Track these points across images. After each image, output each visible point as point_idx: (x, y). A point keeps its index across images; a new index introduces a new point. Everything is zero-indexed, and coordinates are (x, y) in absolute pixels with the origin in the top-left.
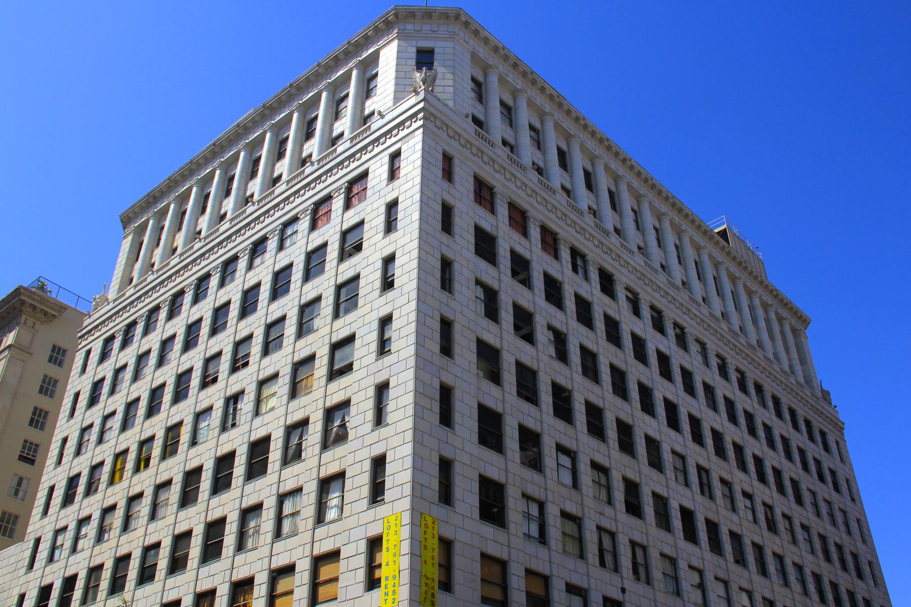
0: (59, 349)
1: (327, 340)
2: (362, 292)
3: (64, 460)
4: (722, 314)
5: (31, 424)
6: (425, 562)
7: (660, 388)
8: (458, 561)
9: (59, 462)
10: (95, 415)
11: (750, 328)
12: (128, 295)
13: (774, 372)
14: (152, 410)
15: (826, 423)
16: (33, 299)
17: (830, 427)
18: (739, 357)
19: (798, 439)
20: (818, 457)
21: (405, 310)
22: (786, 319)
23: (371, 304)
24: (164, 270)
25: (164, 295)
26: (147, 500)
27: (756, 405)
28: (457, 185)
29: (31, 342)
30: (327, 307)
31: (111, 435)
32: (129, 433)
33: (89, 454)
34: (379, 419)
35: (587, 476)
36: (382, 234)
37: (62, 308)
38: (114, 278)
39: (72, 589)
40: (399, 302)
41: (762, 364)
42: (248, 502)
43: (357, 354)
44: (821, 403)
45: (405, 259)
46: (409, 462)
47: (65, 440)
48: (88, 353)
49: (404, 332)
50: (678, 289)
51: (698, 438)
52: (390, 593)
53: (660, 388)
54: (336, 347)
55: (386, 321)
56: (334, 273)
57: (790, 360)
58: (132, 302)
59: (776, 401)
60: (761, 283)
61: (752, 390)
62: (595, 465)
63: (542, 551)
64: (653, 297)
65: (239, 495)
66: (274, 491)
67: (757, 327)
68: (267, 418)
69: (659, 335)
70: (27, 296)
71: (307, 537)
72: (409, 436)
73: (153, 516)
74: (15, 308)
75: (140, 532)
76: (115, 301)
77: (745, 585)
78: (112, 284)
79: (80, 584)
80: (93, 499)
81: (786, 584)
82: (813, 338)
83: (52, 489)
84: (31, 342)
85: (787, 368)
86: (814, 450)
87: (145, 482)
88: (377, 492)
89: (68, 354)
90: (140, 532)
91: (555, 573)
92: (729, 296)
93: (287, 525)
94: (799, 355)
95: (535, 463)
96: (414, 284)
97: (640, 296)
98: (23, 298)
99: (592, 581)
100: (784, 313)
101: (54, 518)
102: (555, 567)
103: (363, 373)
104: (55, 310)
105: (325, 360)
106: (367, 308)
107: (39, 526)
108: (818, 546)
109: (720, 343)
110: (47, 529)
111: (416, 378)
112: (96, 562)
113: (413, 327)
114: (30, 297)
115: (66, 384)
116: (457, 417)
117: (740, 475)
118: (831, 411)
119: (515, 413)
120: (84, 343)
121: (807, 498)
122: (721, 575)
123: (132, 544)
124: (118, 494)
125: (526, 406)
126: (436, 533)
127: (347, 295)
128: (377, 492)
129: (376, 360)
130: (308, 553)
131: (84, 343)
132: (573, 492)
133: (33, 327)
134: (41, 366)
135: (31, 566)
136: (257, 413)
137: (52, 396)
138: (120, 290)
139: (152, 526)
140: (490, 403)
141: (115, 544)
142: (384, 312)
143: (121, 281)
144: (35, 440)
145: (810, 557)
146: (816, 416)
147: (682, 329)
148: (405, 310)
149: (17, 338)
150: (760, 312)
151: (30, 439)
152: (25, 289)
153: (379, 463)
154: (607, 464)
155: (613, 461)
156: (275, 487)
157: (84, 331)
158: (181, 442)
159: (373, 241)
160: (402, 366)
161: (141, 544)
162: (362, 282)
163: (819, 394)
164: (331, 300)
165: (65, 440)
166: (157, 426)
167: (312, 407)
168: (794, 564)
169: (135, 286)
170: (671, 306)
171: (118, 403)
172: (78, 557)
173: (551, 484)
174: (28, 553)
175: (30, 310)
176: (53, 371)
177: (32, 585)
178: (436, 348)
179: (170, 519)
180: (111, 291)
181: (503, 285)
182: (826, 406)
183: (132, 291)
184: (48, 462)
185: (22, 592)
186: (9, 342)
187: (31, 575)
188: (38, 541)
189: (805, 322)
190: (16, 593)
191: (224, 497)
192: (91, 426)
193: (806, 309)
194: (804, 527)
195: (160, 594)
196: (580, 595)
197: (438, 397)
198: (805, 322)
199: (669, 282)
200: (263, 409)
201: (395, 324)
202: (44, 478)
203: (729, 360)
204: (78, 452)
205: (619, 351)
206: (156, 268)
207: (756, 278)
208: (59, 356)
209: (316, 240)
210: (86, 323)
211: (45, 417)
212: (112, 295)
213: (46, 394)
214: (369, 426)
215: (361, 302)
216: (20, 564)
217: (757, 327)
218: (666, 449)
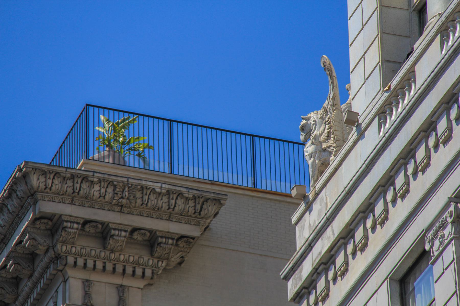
12: (423, 72)
37: (204, 202)
38: (354, 25)
70: (61, 197)
74: (32, 257)
76: (382, 114)
78: (354, 54)
98: (48, 207)
104: (182, 217)
114: (74, 198)
143: (385, 32)
157: (307, 268)
180: (356, 79)
210: (303, 234)
212: (364, 95)
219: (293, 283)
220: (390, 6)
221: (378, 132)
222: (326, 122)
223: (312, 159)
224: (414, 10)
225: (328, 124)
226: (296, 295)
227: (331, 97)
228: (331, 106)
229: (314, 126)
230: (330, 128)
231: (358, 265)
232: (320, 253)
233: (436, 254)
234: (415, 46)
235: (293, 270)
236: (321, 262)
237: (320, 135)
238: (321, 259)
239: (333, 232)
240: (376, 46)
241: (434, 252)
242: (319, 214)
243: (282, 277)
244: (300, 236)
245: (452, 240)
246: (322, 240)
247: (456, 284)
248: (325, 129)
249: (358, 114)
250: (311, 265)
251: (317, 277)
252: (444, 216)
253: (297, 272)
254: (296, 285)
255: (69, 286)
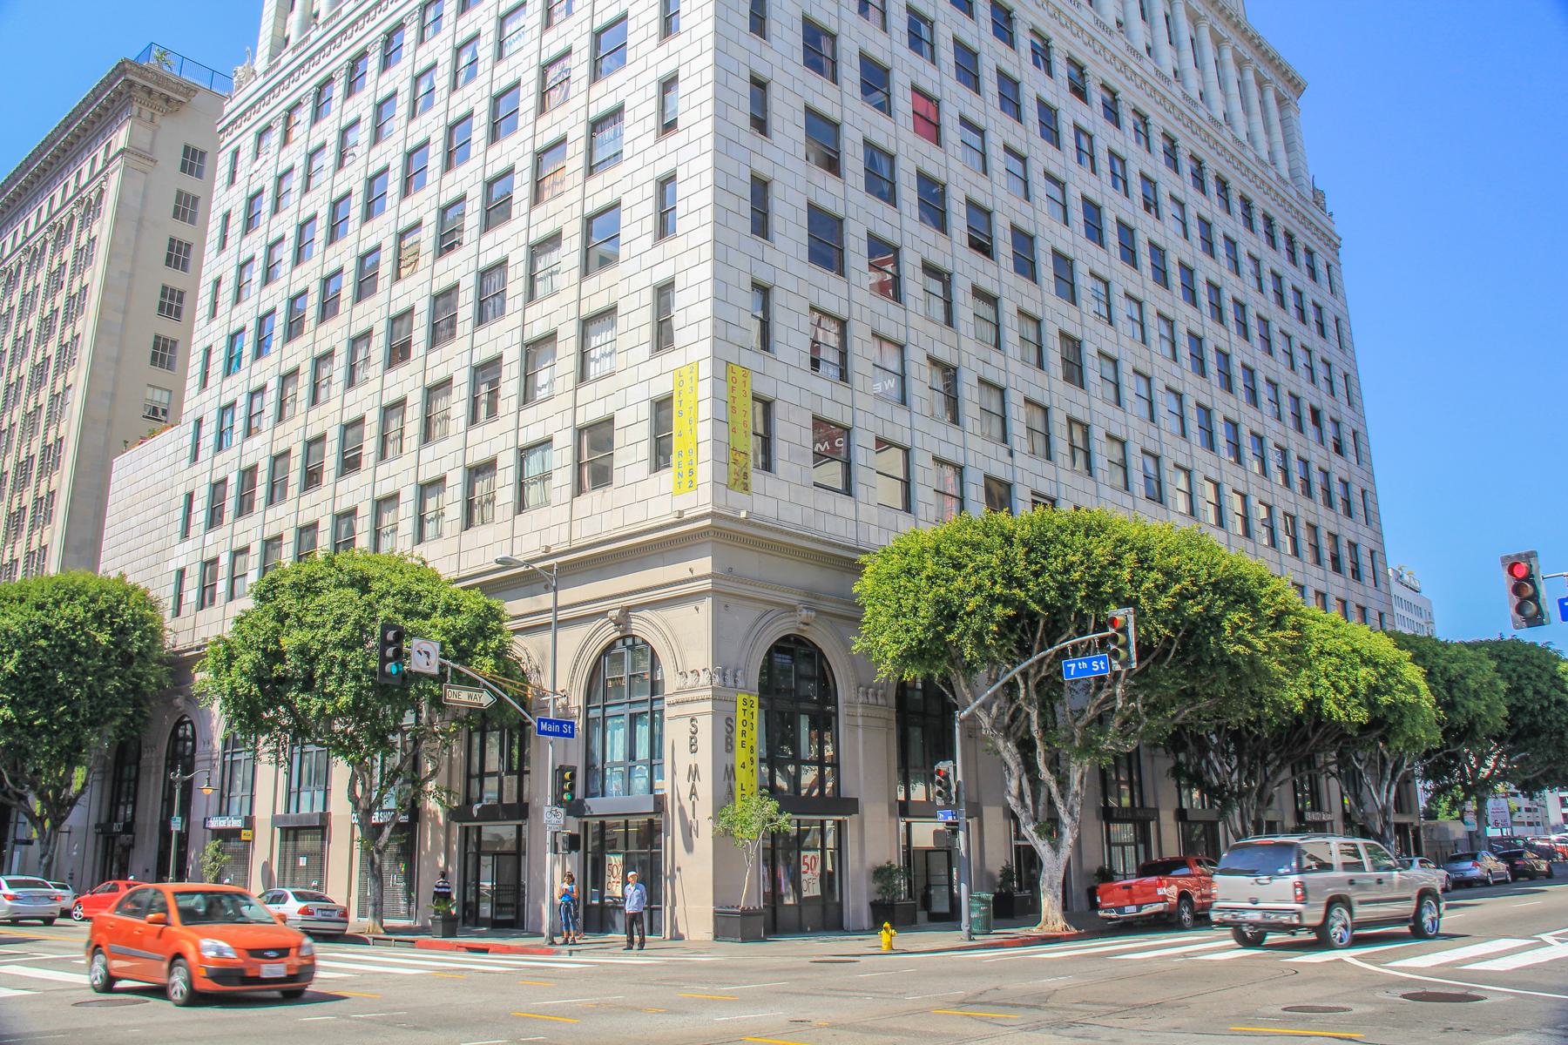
0: (195, 151)
1: (582, 116)
2: (631, 41)
3: (220, 311)
4: (1175, 73)
5: (168, 263)
6: (734, 430)
7: (1078, 182)
8: (780, 429)
9: (213, 314)
10: (255, 245)
11: (1215, 94)
13: (1245, 162)
14: (334, 233)
15: (1315, 238)
16: (146, 78)
17: (1321, 244)
18: (1196, 139)
19: (1275, 260)
20: (1299, 286)
21: (697, 65)
22: (1270, 81)
23: (641, 155)
24: (334, 22)
25: (336, 60)
26: (340, 360)
27: (1217, 210)
28: (775, 41)
29: (152, 145)
30: (579, 65)
31: (291, 201)
32: (305, 267)
33: (253, 301)
34: (664, 228)
35: (965, 307)
36: (655, 40)
37: (191, 90)
39: (253, 485)
40: (684, 155)
41: (1229, 148)
42: (487, 260)
43: (628, 135)
44: (1310, 208)
45: (693, 83)
46: (707, 290)
47: (218, 283)
48: (236, 153)
49: (696, 99)
50: (1110, 33)
51: (1129, 255)
52: (686, 473)
53: (1078, 182)
54: (596, 126)
55: (666, 183)
56: (589, 14)
57: (1270, 144)
58: (292, 74)
59: (1247, 204)
60: (1237, 25)
61: (1212, 187)
62: (978, 293)
63: (901, 416)
64: (1072, 45)
65: (468, 346)
66: (517, 339)
67: (1226, 95)
68: (513, 61)
69: (1077, 102)
70: (136, 74)
71: (567, 401)
72: (707, 252)
73: (351, 382)
75: (335, 404)
76: (265, 73)
77: (1183, 462)
79: (262, 478)
80: (264, 363)
81: (1239, 460)
82: (1307, 111)
83: (208, 351)
84: (152, 145)
85: (1265, 157)
86: (1295, 277)
87: (334, 335)
88: (663, 337)
89: (208, 158)
90: (335, 404)
91: (918, 443)
92: (1187, 45)
93: (533, 493)
94: (1285, 136)
95: (893, 289)
96: (709, 26)
97: (1052, 43)
98: (130, 77)
99: (971, 455)
100: (1268, 73)
101: (216, 390)
102: (917, 435)
103: (636, 163)
104: (181, 94)
105: (581, 146)
106: (640, 65)
107: (199, 403)
108: (1287, 409)
109: (1170, 117)
110: (209, 406)
111: (716, 168)
112: (280, 447)
113: (709, 58)
115: (190, 345)
116: (776, 224)
117: (1187, 309)
118: (1325, 221)
119: (863, 216)
120: (228, 140)
121: (1279, 343)
122: (1151, 447)
123: (327, 419)
124: (298, 354)
125: (879, 207)
126: (748, 389)
127: (599, 243)
128: (663, 337)
129: (659, 46)
130: (569, 422)
131: (228, 140)
132: (947, 331)
133: (152, 121)
134: (171, 180)
135: (195, 457)
136: (500, 56)
137: (170, 367)
138: (272, 56)
139: (351, 396)
140: (825, 202)
141: (302, 422)
142: (665, 70)
144: (178, 286)
145: (1275, 425)
146: (1301, 227)
147: (1114, 94)
148: (697, 65)
149: (131, 137)
150: (1231, 71)
151: (171, 284)
152: (131, 63)
153: (664, 291)
154: (989, 206)
155: (1005, 287)
156: (517, 333)
158: (380, 276)
159: (643, 49)
160: (693, 150)
161: (337, 421)
162: (631, 25)
163: (1309, 195)
164: (586, 54)
165: (218, 283)
166: (344, 255)
167: (572, 120)
168: (1244, 366)
169: (294, 50)
170: (1100, 59)
171: (285, 225)
172: (256, 441)
173: (915, 320)
174: (189, 440)
175: (145, 96)
176: (190, 184)
177: (199, 480)
178: (744, 121)
179: (374, 385)
180: (258, 58)
181: (845, 26)
182: (1316, 213)
183: (289, 57)
184: (198, 315)
185: (189, 490)
186: (120, 146)
187: (197, 468)
188: (199, 422)
189: (1298, 87)
190: (181, 491)
191: (446, 351)
192: (261, 192)
193: (1300, 70)
194: (1273, 384)
195: (369, 487)
196: (942, 280)
197: (748, 195)
198: (1298, 87)
199: (1097, 22)
200: (507, 52)
201: (683, 88)
202: (196, 338)
203: (1181, 142)
204: (238, 300)
205: (1018, 127)
206: (321, 20)
207: (1229, 18)
208: (194, 161)
209: (554, 44)
210: (227, 110)
211: (187, 253)
213: (191, 173)
214: (649, 239)
215: (630, 55)
216: (180, 454)
217: (1226, 95)
218: (1081, 270)
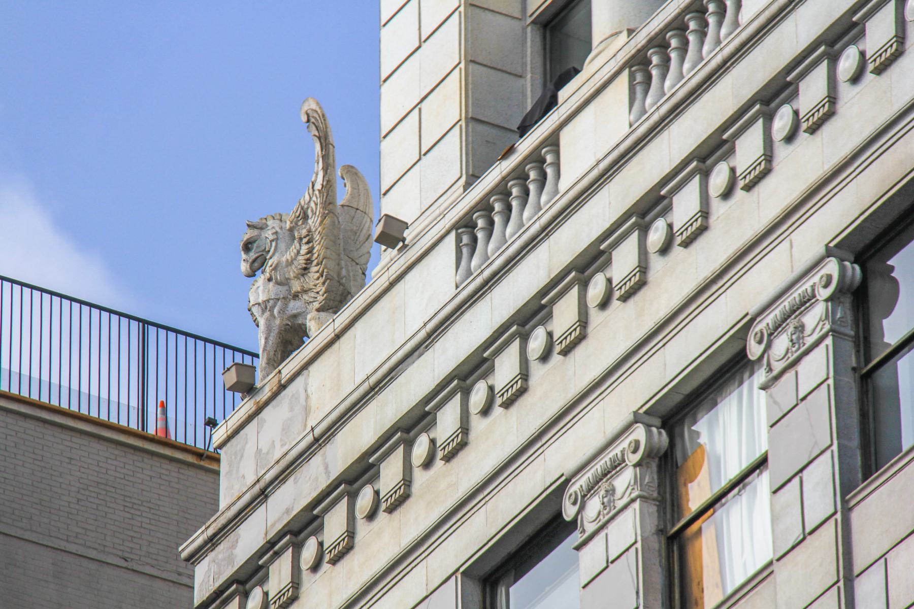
219: (209, 570)
220: (485, 6)
221: (454, 266)
222: (301, 239)
223: (267, 314)
224: (533, 22)
225: (308, 243)
226: (214, 595)
227: (318, 186)
228: (316, 204)
229: (274, 244)
230: (310, 251)
231: (381, 542)
232: (288, 511)
233: (590, 528)
234: (563, 94)
235: (212, 542)
236: (286, 529)
237: (290, 263)
238: (289, 523)
239: (326, 468)
240: (453, 88)
241: (585, 523)
242: (286, 429)
243: (184, 555)
244: (229, 472)
245: (633, 501)
246: (295, 483)
247: (637, 593)
248: (298, 252)
249: (406, 226)
250: (264, 536)
251: (272, 560)
252: (620, 448)
253: (221, 547)
254: (220, 574)
255: (874, 388)
